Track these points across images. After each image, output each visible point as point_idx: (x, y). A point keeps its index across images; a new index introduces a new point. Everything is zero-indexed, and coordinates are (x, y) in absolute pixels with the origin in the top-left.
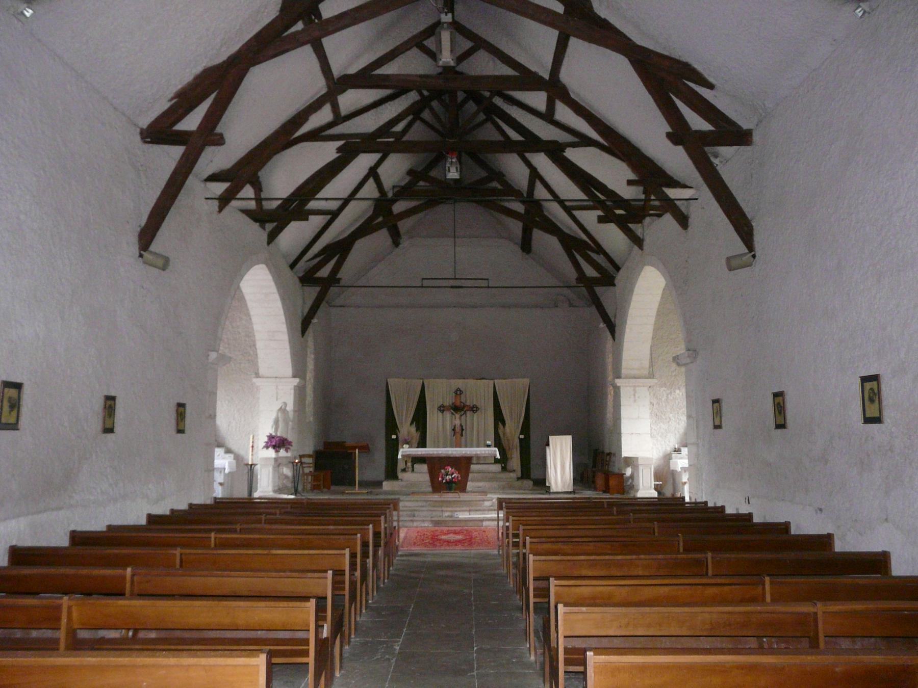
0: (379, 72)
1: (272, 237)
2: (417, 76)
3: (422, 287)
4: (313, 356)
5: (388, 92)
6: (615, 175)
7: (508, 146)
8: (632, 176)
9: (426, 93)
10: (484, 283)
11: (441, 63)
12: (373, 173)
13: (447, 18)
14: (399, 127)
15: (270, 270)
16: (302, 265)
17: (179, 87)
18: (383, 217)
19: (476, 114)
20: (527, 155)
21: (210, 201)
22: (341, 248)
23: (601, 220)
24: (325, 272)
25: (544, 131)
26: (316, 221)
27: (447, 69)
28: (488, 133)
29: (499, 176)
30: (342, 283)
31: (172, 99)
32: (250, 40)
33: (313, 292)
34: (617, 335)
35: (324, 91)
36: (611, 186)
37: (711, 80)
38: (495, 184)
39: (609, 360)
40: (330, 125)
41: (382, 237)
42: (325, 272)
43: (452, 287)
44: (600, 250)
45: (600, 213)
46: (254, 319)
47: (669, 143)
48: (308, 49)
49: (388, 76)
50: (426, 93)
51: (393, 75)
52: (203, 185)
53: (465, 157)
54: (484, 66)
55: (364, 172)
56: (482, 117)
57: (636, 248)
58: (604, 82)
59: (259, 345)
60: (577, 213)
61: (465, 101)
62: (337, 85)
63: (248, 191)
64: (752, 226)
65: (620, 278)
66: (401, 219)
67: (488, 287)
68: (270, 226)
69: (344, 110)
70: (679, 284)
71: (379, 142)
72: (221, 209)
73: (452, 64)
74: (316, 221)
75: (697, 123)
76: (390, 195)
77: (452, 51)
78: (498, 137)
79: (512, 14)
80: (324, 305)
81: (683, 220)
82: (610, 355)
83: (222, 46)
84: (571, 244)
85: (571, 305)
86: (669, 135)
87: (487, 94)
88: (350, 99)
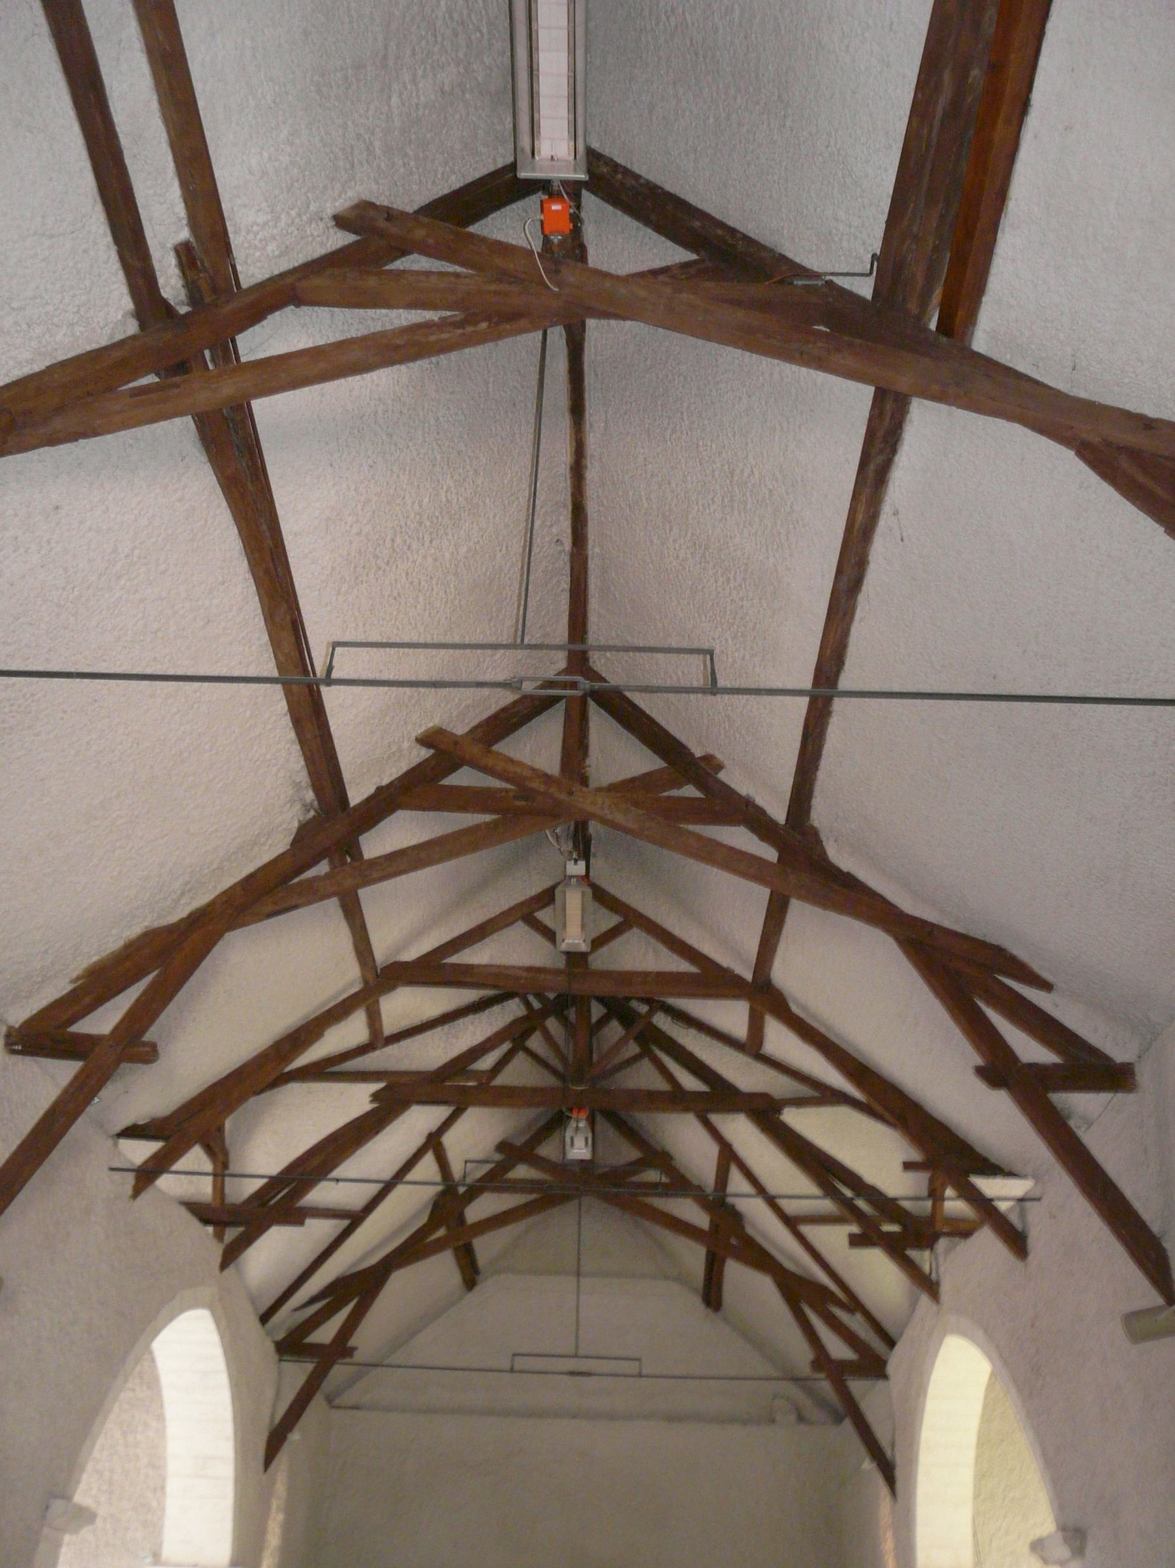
0: (454, 959)
1: (231, 1255)
2: (520, 968)
3: (512, 1370)
4: (281, 1517)
5: (469, 996)
6: (878, 1156)
7: (677, 1099)
8: (915, 1156)
9: (536, 1005)
10: (631, 1367)
11: (564, 947)
12: (433, 1142)
13: (579, 868)
14: (487, 1062)
15: (217, 1323)
16: (286, 1318)
17: (95, 959)
18: (448, 1226)
19: (623, 1041)
20: (715, 1118)
21: (117, 1175)
22: (362, 1287)
23: (856, 1241)
24: (325, 1334)
25: (745, 1075)
26: (320, 1230)
27: (576, 959)
28: (645, 1077)
29: (660, 1158)
30: (358, 1356)
31: (78, 978)
32: (233, 887)
33: (298, 1372)
34: (899, 1485)
35: (356, 988)
36: (870, 1176)
37: (1046, 975)
38: (652, 1176)
39: (888, 1545)
40: (362, 1050)
41: (442, 1268)
42: (325, 1334)
43: (572, 1373)
44: (855, 1304)
45: (855, 1229)
46: (173, 1428)
47: (980, 1086)
48: (332, 905)
49: (472, 967)
50: (536, 1005)
51: (479, 966)
52: (110, 1142)
53: (601, 1123)
54: (637, 955)
55: (418, 1141)
56: (633, 1049)
57: (925, 1299)
58: (851, 982)
59: (173, 1486)
60: (805, 1229)
61: (603, 1021)
62: (384, 978)
63: (196, 1158)
64: (1164, 1250)
65: (896, 1362)
66: (482, 1232)
67: (640, 1375)
68: (231, 1234)
69: (389, 1026)
70: (1030, 1373)
71: (452, 1086)
72: (137, 1192)
73: (584, 947)
74: (320, 1230)
75: (1030, 1050)
76: (356, 795)
77: (583, 926)
78: (662, 1085)
79: (691, 861)
80: (317, 1403)
81: (1016, 1240)
82: (889, 1535)
83: (183, 894)
84: (798, 1291)
85: (801, 1419)
86: (980, 1072)
87: (643, 1009)
88: (404, 1005)
